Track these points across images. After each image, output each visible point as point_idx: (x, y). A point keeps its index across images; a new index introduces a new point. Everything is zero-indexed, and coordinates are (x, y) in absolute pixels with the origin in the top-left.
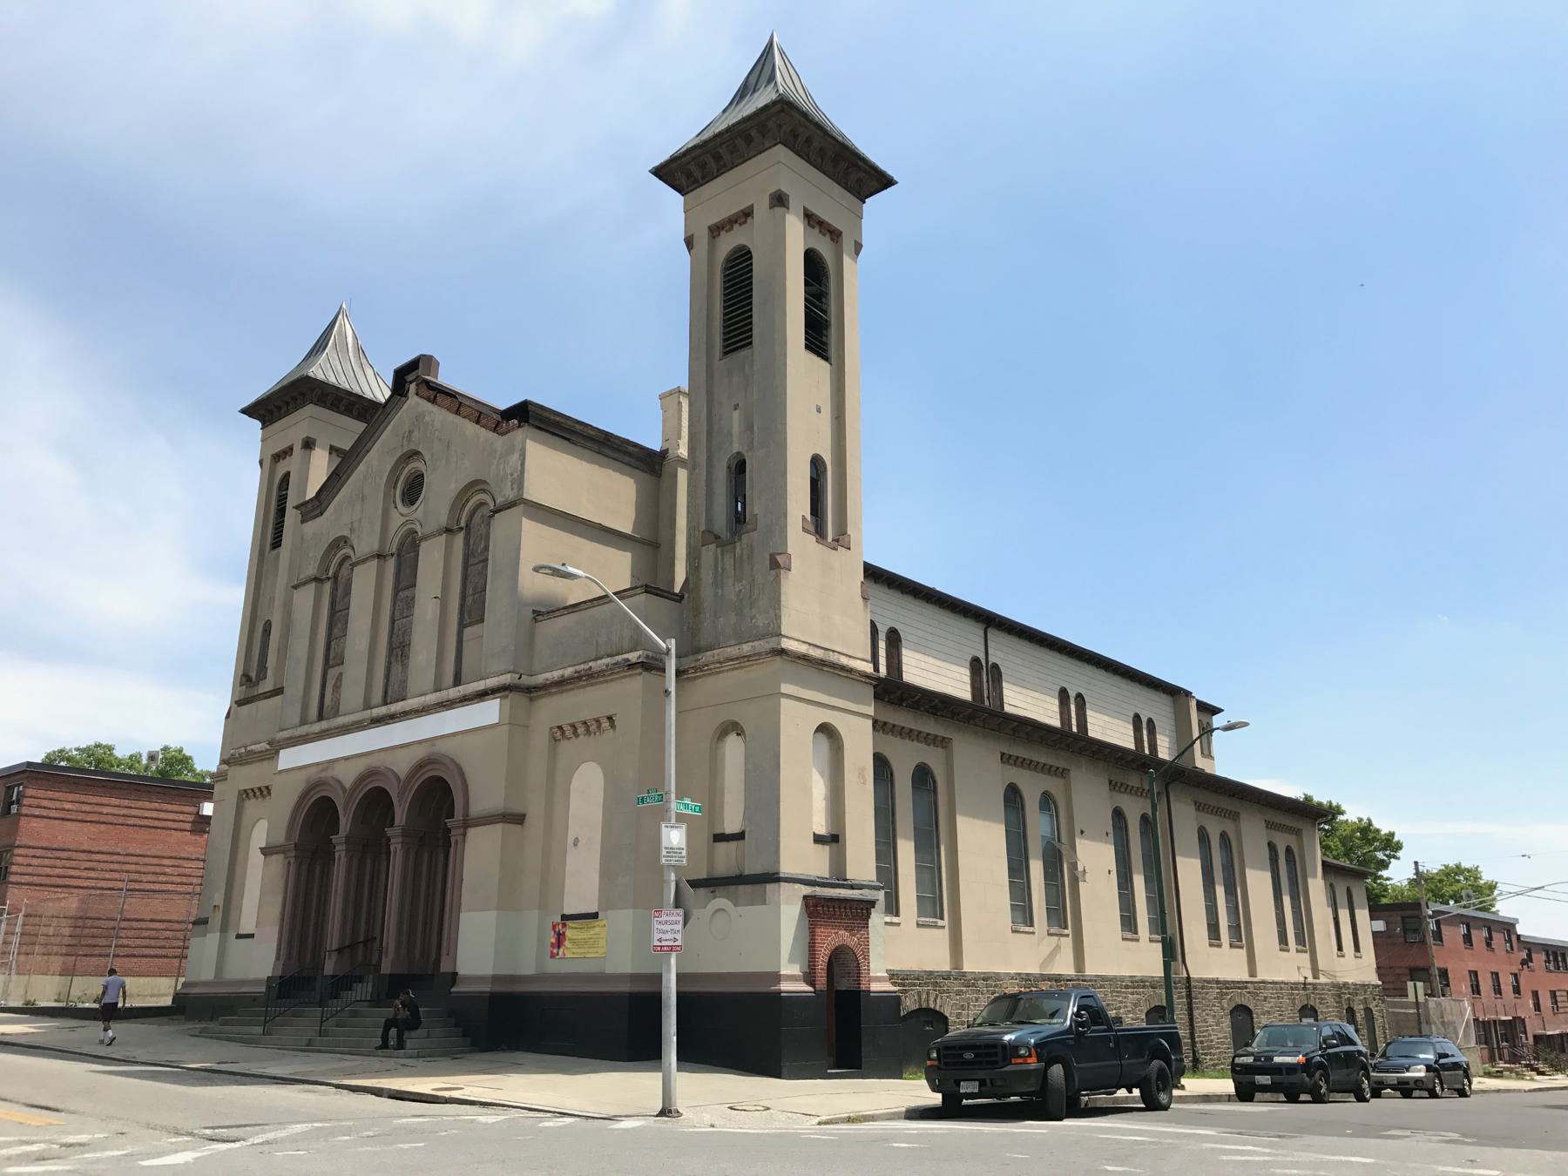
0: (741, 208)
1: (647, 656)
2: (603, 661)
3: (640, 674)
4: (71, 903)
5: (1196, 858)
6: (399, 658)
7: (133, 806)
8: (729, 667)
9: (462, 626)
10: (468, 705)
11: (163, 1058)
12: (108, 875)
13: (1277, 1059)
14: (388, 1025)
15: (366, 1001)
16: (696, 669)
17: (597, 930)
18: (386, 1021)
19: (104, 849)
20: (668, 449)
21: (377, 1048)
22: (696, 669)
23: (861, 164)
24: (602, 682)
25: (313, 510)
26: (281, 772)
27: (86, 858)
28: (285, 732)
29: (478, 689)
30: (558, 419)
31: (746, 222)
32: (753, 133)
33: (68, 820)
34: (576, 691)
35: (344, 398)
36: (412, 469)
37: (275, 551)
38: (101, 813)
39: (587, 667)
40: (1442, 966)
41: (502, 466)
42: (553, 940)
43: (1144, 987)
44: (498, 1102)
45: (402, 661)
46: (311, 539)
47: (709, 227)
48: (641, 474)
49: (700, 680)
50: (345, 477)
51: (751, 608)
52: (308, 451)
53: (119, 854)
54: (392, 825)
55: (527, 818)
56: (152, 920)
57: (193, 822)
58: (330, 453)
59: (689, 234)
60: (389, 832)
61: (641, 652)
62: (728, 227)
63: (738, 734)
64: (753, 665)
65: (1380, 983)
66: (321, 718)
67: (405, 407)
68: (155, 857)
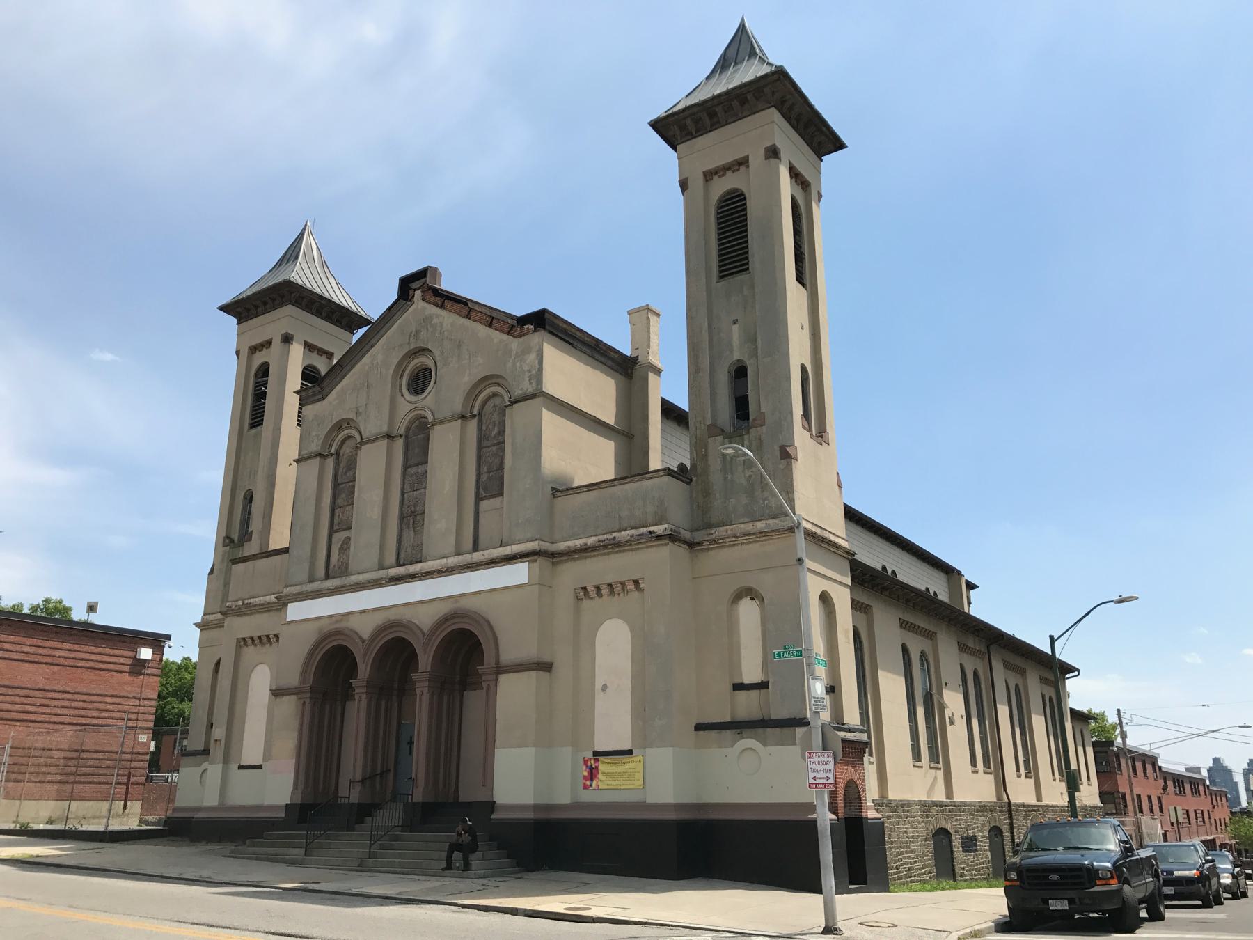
0: (737, 158)
1: (671, 530)
2: (627, 532)
3: (666, 544)
4: (64, 737)
5: (1005, 705)
6: (411, 526)
7: (81, 650)
9: (478, 499)
10: (493, 567)
11: (243, 879)
12: (59, 711)
13: (1177, 873)
14: (453, 847)
15: (398, 826)
16: (710, 542)
17: (632, 765)
18: (450, 845)
19: (56, 688)
20: (638, 356)
21: (443, 870)
22: (710, 542)
23: (824, 129)
24: (628, 550)
25: (314, 395)
26: (289, 623)
27: (41, 696)
28: (292, 588)
29: (506, 553)
30: (565, 326)
31: (738, 170)
32: (749, 96)
33: (26, 661)
34: (600, 558)
36: (418, 364)
37: (254, 431)
38: (54, 656)
39: (610, 537)
40: (1138, 793)
42: (586, 774)
43: (986, 810)
46: (312, 420)
47: (704, 172)
48: (620, 376)
50: (348, 368)
51: (762, 492)
52: (287, 344)
53: (68, 692)
54: (416, 670)
55: (554, 666)
56: (96, 751)
57: (131, 665)
58: (304, 348)
59: (684, 177)
60: (415, 677)
61: (666, 526)
62: (722, 173)
63: (752, 599)
65: (1102, 805)
66: (327, 576)
67: (410, 310)
68: (98, 695)
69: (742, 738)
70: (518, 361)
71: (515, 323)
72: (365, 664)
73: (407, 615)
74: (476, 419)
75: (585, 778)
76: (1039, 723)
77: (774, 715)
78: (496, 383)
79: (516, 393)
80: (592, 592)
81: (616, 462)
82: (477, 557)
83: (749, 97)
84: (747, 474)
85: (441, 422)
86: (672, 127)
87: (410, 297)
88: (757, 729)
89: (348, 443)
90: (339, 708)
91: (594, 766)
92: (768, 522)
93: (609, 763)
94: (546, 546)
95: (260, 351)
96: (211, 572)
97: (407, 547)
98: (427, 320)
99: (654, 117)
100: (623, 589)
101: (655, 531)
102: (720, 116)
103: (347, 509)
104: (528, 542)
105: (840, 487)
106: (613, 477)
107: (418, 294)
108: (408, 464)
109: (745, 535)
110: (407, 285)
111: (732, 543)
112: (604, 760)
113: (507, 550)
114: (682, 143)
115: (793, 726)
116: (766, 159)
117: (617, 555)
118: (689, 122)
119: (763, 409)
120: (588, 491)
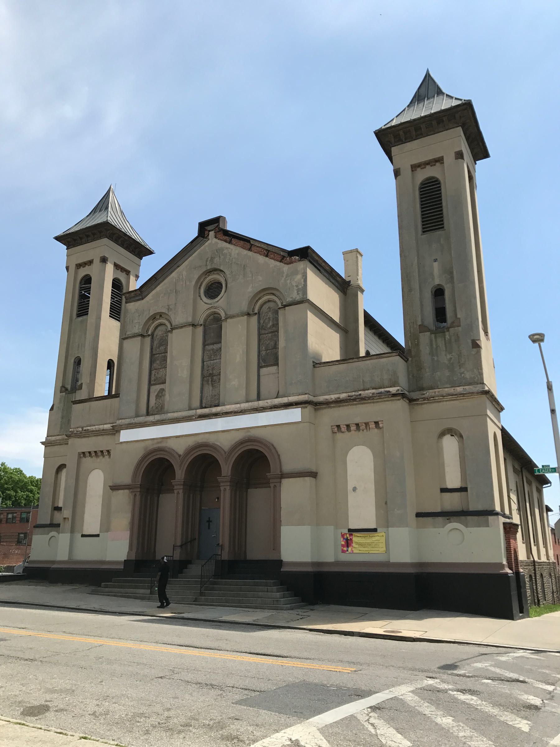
2: (370, 391)
3: (399, 400)
6: (210, 383)
8: (448, 399)
9: (260, 367)
17: (379, 538)
22: (424, 399)
23: (481, 144)
24: (370, 403)
28: (123, 421)
29: (284, 402)
32: (444, 119)
35: (122, 237)
37: (80, 319)
39: (357, 393)
41: (288, 281)
42: (343, 543)
44: (472, 642)
45: (212, 384)
47: (411, 165)
49: (425, 405)
50: (161, 280)
51: (460, 368)
52: (104, 263)
60: (219, 479)
61: (399, 388)
63: (452, 435)
64: (465, 399)
66: (148, 414)
67: (207, 244)
69: (450, 522)
70: (288, 280)
71: (286, 255)
72: (181, 471)
73: (212, 440)
74: (257, 316)
75: (343, 546)
76: (537, 511)
77: (471, 509)
78: (271, 293)
79: (287, 300)
80: (344, 428)
81: (340, 347)
82: (261, 403)
83: (444, 119)
84: (449, 357)
85: (232, 317)
86: (389, 135)
87: (206, 236)
88: (461, 517)
89: (159, 328)
90: (156, 498)
91: (349, 538)
92: (465, 387)
93: (360, 537)
94: (311, 398)
95: (83, 267)
96: (52, 409)
97: (207, 397)
98: (220, 251)
99: (378, 128)
100: (366, 427)
101: (390, 391)
102: (423, 130)
103: (161, 371)
104: (299, 395)
105: (494, 367)
106: (339, 359)
107: (212, 234)
108: (206, 343)
109: (449, 395)
110: (204, 227)
111: (439, 400)
112: (356, 535)
113: (285, 400)
114: (395, 146)
115: (486, 515)
116: (456, 159)
117: (362, 405)
118: (401, 133)
119: (459, 316)
120: (340, 364)
